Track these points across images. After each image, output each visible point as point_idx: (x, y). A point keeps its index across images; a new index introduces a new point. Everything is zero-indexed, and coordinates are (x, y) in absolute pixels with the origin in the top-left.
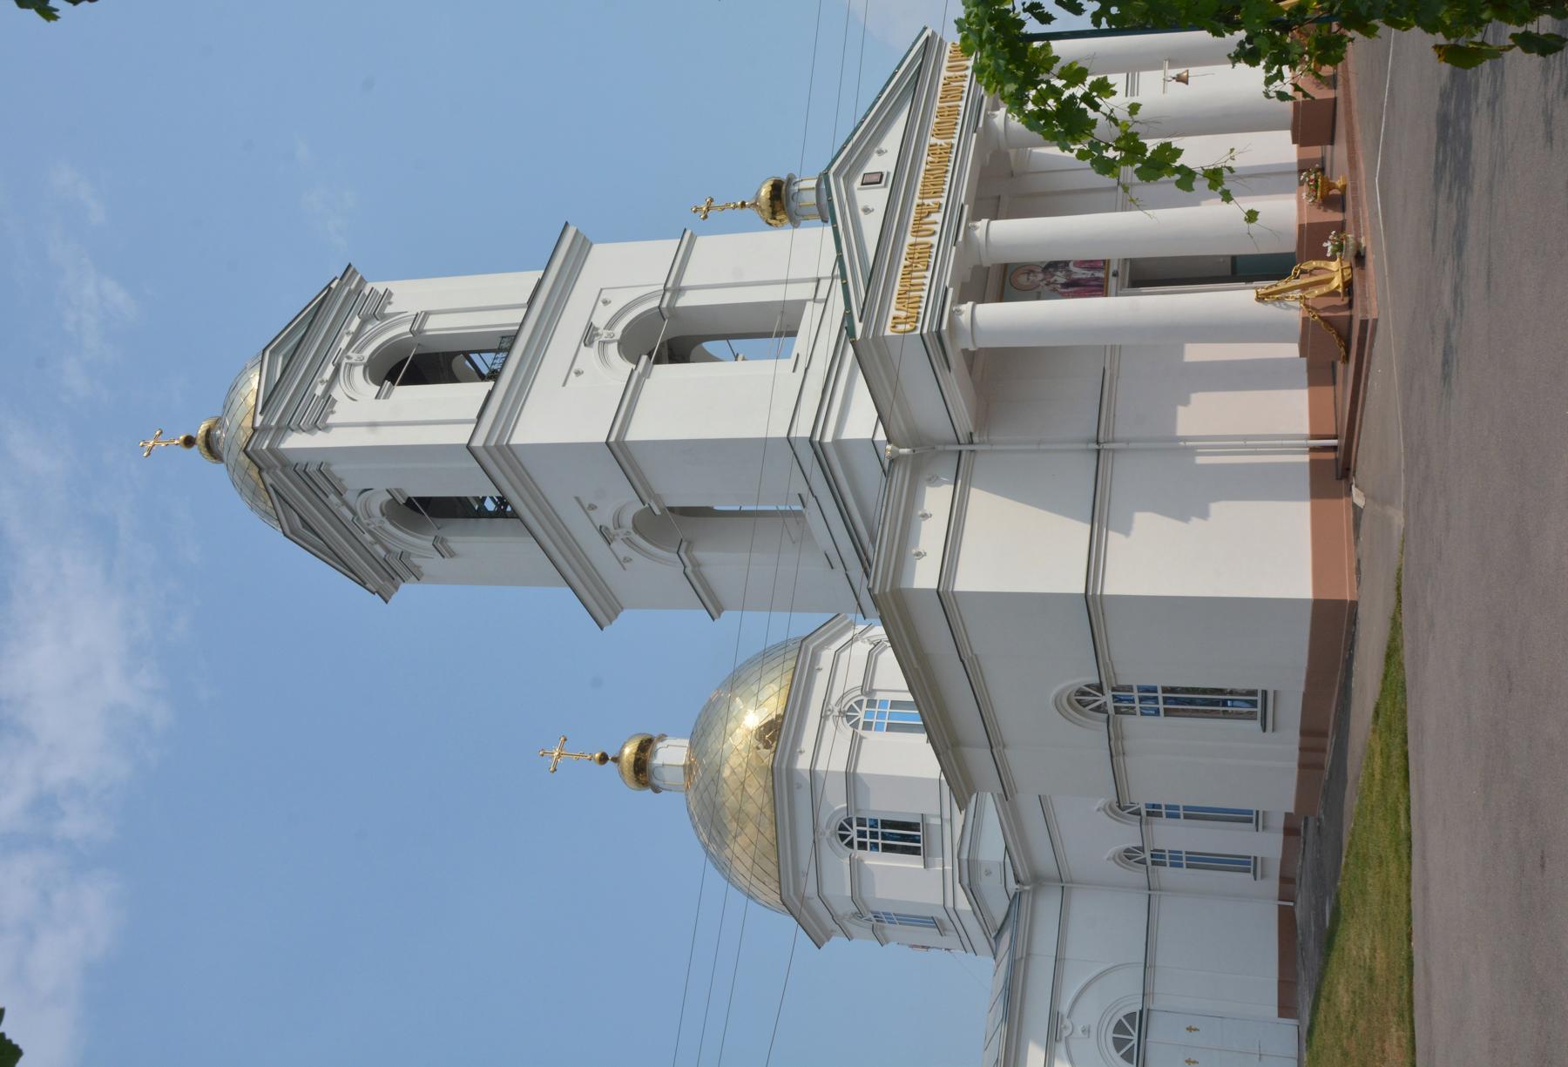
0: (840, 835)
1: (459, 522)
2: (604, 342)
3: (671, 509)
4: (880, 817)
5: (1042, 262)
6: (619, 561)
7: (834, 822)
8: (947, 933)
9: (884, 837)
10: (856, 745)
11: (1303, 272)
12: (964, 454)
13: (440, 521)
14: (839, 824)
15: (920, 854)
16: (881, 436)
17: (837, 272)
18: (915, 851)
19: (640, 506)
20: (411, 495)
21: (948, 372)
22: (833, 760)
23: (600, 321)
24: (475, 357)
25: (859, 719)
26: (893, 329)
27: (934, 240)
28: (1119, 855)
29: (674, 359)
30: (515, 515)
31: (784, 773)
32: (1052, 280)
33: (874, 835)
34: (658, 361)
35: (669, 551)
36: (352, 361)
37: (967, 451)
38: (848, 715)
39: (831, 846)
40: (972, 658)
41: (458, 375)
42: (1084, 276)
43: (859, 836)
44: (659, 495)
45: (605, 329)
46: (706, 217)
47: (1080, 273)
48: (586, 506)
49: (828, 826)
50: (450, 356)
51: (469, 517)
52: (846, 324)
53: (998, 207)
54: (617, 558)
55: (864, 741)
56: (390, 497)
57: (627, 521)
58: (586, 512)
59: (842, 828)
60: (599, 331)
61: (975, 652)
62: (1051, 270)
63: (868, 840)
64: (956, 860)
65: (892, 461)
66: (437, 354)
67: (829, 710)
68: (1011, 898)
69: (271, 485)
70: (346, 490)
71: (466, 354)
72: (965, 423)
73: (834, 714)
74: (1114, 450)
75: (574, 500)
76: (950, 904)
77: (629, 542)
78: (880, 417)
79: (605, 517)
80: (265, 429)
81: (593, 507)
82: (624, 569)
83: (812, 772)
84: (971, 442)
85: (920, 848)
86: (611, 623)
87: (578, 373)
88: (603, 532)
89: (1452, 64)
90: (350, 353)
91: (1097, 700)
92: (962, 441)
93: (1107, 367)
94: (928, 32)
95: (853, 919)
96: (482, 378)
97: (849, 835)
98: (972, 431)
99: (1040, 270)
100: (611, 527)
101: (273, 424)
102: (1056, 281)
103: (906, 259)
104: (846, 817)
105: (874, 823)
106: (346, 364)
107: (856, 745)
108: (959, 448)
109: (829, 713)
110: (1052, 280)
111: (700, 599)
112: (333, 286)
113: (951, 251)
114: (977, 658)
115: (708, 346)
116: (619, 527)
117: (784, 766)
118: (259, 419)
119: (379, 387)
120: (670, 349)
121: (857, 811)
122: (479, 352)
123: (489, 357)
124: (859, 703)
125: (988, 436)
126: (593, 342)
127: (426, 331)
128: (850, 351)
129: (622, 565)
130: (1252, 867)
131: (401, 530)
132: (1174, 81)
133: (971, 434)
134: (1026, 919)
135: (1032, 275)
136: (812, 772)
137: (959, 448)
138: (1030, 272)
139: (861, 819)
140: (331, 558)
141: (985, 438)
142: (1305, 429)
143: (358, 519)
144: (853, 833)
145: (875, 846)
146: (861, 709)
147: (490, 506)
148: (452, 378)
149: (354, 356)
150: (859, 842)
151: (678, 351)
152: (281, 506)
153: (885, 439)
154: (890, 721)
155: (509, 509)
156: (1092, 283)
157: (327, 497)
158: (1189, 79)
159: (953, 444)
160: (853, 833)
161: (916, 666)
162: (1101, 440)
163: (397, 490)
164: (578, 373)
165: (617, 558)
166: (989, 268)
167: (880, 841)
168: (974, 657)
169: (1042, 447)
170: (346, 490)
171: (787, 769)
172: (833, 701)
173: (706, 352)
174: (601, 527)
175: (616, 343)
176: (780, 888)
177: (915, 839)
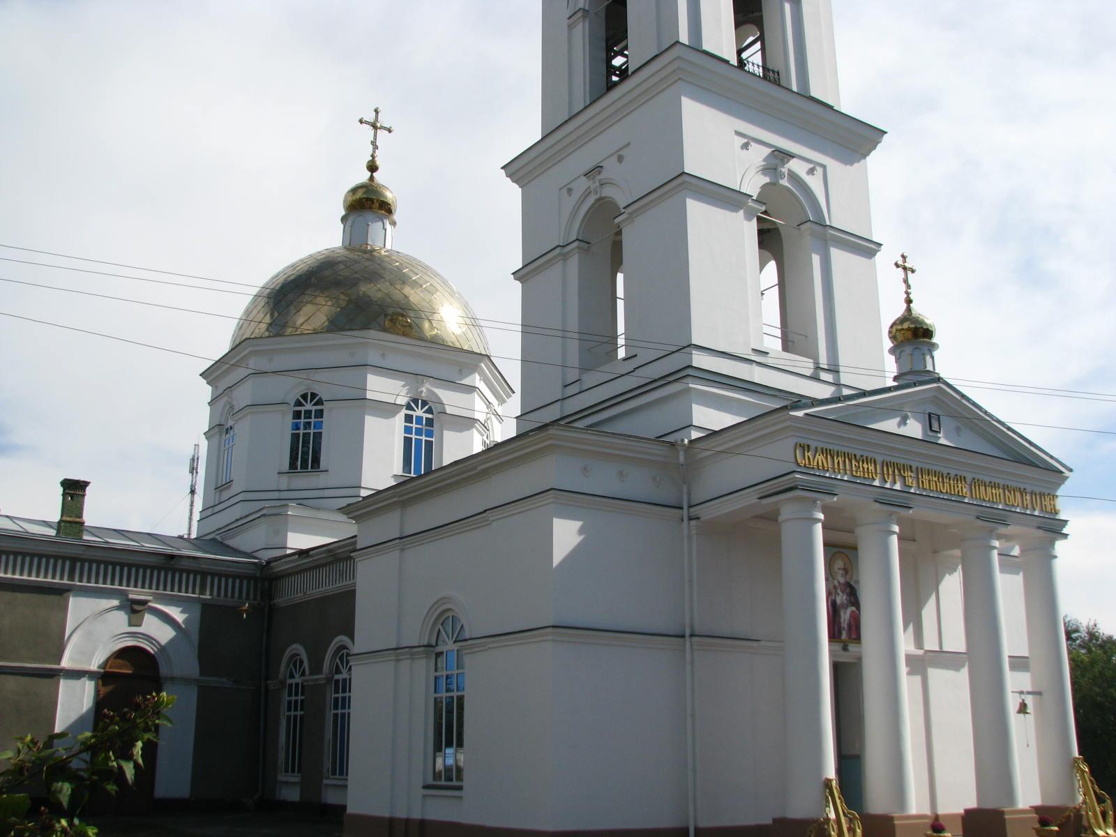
0: (306, 394)
1: (603, 34)
3: (619, 233)
4: (325, 431)
5: (857, 582)
6: (569, 184)
8: (218, 493)
11: (851, 821)
12: (680, 511)
13: (603, 15)
15: (290, 469)
16: (695, 435)
17: (846, 392)
18: (293, 465)
19: (622, 204)
21: (758, 496)
24: (758, 46)
25: (415, 411)
26: (798, 445)
27: (877, 483)
28: (298, 655)
29: (761, 232)
30: (611, 86)
32: (839, 591)
33: (308, 425)
34: (759, 219)
35: (578, 232)
37: (683, 515)
40: (488, 520)
41: (741, 28)
42: (842, 620)
43: (305, 411)
44: (633, 221)
45: (789, 169)
46: (897, 265)
47: (845, 616)
48: (621, 153)
50: (759, 23)
51: (607, 41)
52: (804, 401)
53: (909, 540)
54: (572, 181)
57: (608, 192)
58: (617, 151)
59: (314, 395)
62: (848, 590)
65: (672, 444)
66: (760, 10)
68: (254, 554)
71: (761, 39)
72: (706, 512)
74: (684, 651)
77: (587, 193)
78: (715, 433)
79: (612, 170)
81: (620, 159)
82: (560, 189)
84: (690, 519)
85: (297, 469)
88: (598, 168)
89: (287, 532)
91: (449, 639)
92: (692, 510)
93: (762, 643)
94: (1067, 473)
95: (228, 406)
96: (739, 52)
97: (307, 402)
99: (848, 580)
100: (600, 177)
102: (838, 594)
103: (862, 456)
108: (685, 506)
110: (839, 591)
111: (541, 257)
115: (772, 266)
116: (602, 185)
120: (768, 231)
122: (763, 49)
123: (758, 59)
128: (776, 405)
129: (563, 187)
132: (1021, 701)
133: (698, 518)
135: (843, 572)
137: (685, 506)
138: (846, 571)
139: (322, 414)
144: (309, 406)
145: (296, 427)
146: (424, 412)
147: (618, 61)
148: (738, 24)
150: (300, 412)
151: (769, 239)
153: (693, 438)
154: (316, 431)
155: (615, 79)
156: (836, 628)
158: (1022, 715)
159: (689, 503)
160: (419, 412)
165: (572, 181)
166: (853, 532)
167: (301, 431)
168: (489, 522)
173: (767, 263)
174: (601, 167)
176: (256, 338)
177: (304, 466)
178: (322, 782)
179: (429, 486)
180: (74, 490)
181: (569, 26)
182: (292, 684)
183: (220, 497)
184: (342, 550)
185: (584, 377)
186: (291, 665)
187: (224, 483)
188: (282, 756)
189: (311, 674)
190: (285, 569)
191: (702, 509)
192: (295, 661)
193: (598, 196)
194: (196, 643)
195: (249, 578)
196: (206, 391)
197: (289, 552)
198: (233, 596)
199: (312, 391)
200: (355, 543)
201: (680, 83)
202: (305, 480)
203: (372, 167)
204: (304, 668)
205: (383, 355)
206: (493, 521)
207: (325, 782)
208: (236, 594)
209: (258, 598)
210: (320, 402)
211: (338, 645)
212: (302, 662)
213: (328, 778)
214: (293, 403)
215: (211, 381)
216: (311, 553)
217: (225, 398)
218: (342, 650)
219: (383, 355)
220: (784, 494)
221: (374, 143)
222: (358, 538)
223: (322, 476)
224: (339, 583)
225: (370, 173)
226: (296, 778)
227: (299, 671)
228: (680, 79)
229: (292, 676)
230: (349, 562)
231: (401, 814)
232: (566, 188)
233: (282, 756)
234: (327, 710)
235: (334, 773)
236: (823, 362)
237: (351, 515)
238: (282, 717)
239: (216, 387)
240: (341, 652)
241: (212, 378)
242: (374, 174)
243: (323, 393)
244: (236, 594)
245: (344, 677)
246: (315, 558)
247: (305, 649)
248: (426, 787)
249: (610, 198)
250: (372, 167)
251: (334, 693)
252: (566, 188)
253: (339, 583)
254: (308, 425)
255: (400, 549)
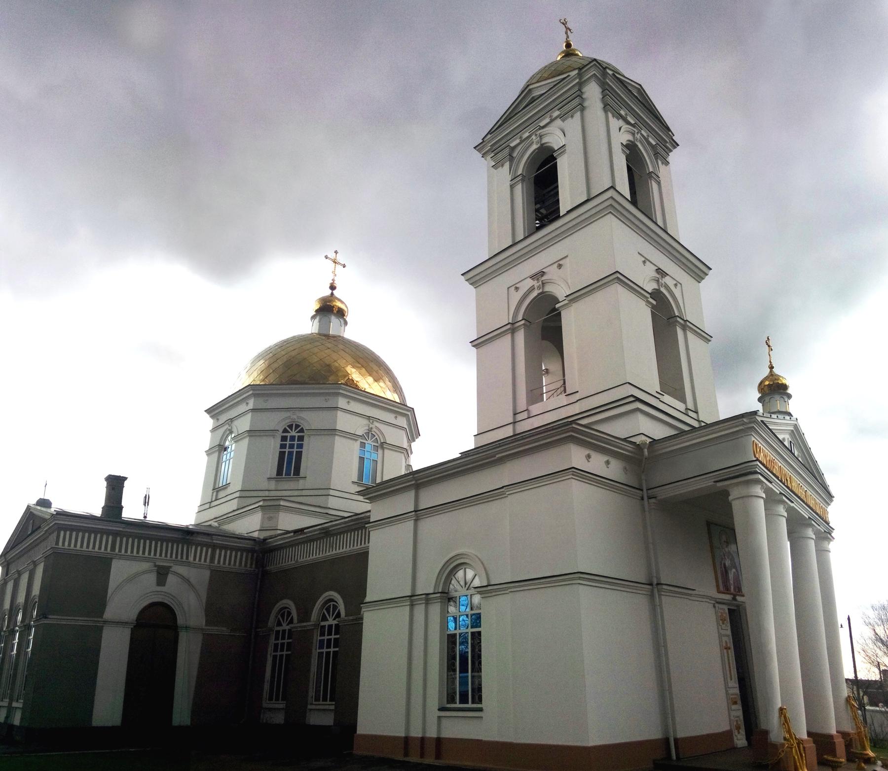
2: (658, 281)
4: (304, 450)
7: (302, 422)
9: (290, 453)
10: (352, 436)
12: (641, 492)
14: (300, 424)
15: (277, 475)
18: (279, 472)
20: (558, 161)
22: (344, 422)
23: (667, 280)
28: (286, 608)
31: (336, 391)
33: (292, 446)
36: (636, 135)
38: (369, 433)
39: (284, 419)
42: (730, 578)
43: (290, 436)
49: (298, 417)
55: (272, 438)
56: (556, 149)
57: (548, 288)
59: (297, 426)
60: (663, 279)
61: (509, 496)
63: (288, 443)
64: (280, 498)
67: (373, 422)
69: (569, 76)
70: (563, 121)
73: (370, 424)
75: (711, 267)
76: (332, 492)
77: (532, 289)
79: (552, 273)
80: (605, 74)
81: (560, 266)
83: (336, 408)
84: (649, 498)
85: (282, 475)
86: (467, 280)
87: (644, 262)
88: (542, 273)
90: (639, 135)
92: (650, 492)
97: (292, 430)
98: (659, 498)
100: (543, 278)
101: (607, 80)
104: (305, 429)
105: (300, 446)
106: (635, 131)
107: (352, 436)
108: (645, 490)
109: (371, 421)
112: (670, 133)
113: (778, 490)
114: (505, 497)
117: (341, 391)
118: (610, 72)
119: (625, 144)
121: (309, 436)
124: (376, 440)
125: (654, 509)
126: (659, 274)
127: (651, 180)
130: (470, 705)
131: (527, 160)
133: (655, 498)
134: (559, 475)
136: (336, 408)
137: (645, 490)
140: (510, 113)
141: (653, 507)
142: (681, 734)
143: (539, 129)
144: (293, 433)
145: (283, 446)
149: (638, 136)
152: (552, 82)
157: (558, 110)
161: (497, 456)
162: (659, 587)
163: (565, 150)
164: (644, 262)
167: (287, 450)
169: (651, 546)
170: (563, 121)
171: (339, 393)
172: (377, 424)
175: (658, 288)
177: (288, 474)
178: (307, 707)
179: (431, 476)
180: (116, 484)
181: (511, 186)
182: (279, 631)
183: (217, 495)
184: (334, 528)
185: (531, 408)
186: (279, 616)
187: (221, 485)
188: (266, 686)
189: (300, 621)
190: (280, 544)
191: (662, 490)
192: (285, 613)
193: (541, 291)
194: (204, 601)
195: (248, 551)
196: (209, 423)
197: (279, 532)
198: (235, 564)
199: (296, 423)
200: (369, 517)
201: (610, 214)
202: (288, 485)
203: (333, 287)
204: (292, 616)
205: (349, 402)
206: (509, 494)
207: (309, 707)
208: (237, 564)
209: (254, 566)
210: (302, 431)
211: (328, 598)
212: (289, 613)
213: (312, 704)
214: (281, 430)
215: (213, 416)
216: (305, 531)
217: (227, 427)
218: (330, 602)
219: (349, 402)
220: (722, 482)
221: (334, 272)
222: (371, 514)
223: (301, 481)
224: (329, 552)
225: (331, 291)
226: (281, 705)
227: (286, 621)
228: (610, 212)
229: (279, 624)
230: (342, 537)
231: (416, 732)
232: (556, 264)
233: (266, 686)
234: (314, 650)
235: (317, 699)
236: (690, 405)
237: (367, 497)
238: (269, 656)
239: (218, 419)
240: (329, 604)
241: (213, 414)
242: (334, 292)
243: (305, 426)
244: (237, 564)
245: (283, 629)
246: (308, 535)
247: (295, 603)
248: (442, 709)
249: (549, 292)
250: (333, 287)
251: (320, 636)
252: (556, 264)
253: (329, 552)
254: (292, 446)
255: (414, 520)
